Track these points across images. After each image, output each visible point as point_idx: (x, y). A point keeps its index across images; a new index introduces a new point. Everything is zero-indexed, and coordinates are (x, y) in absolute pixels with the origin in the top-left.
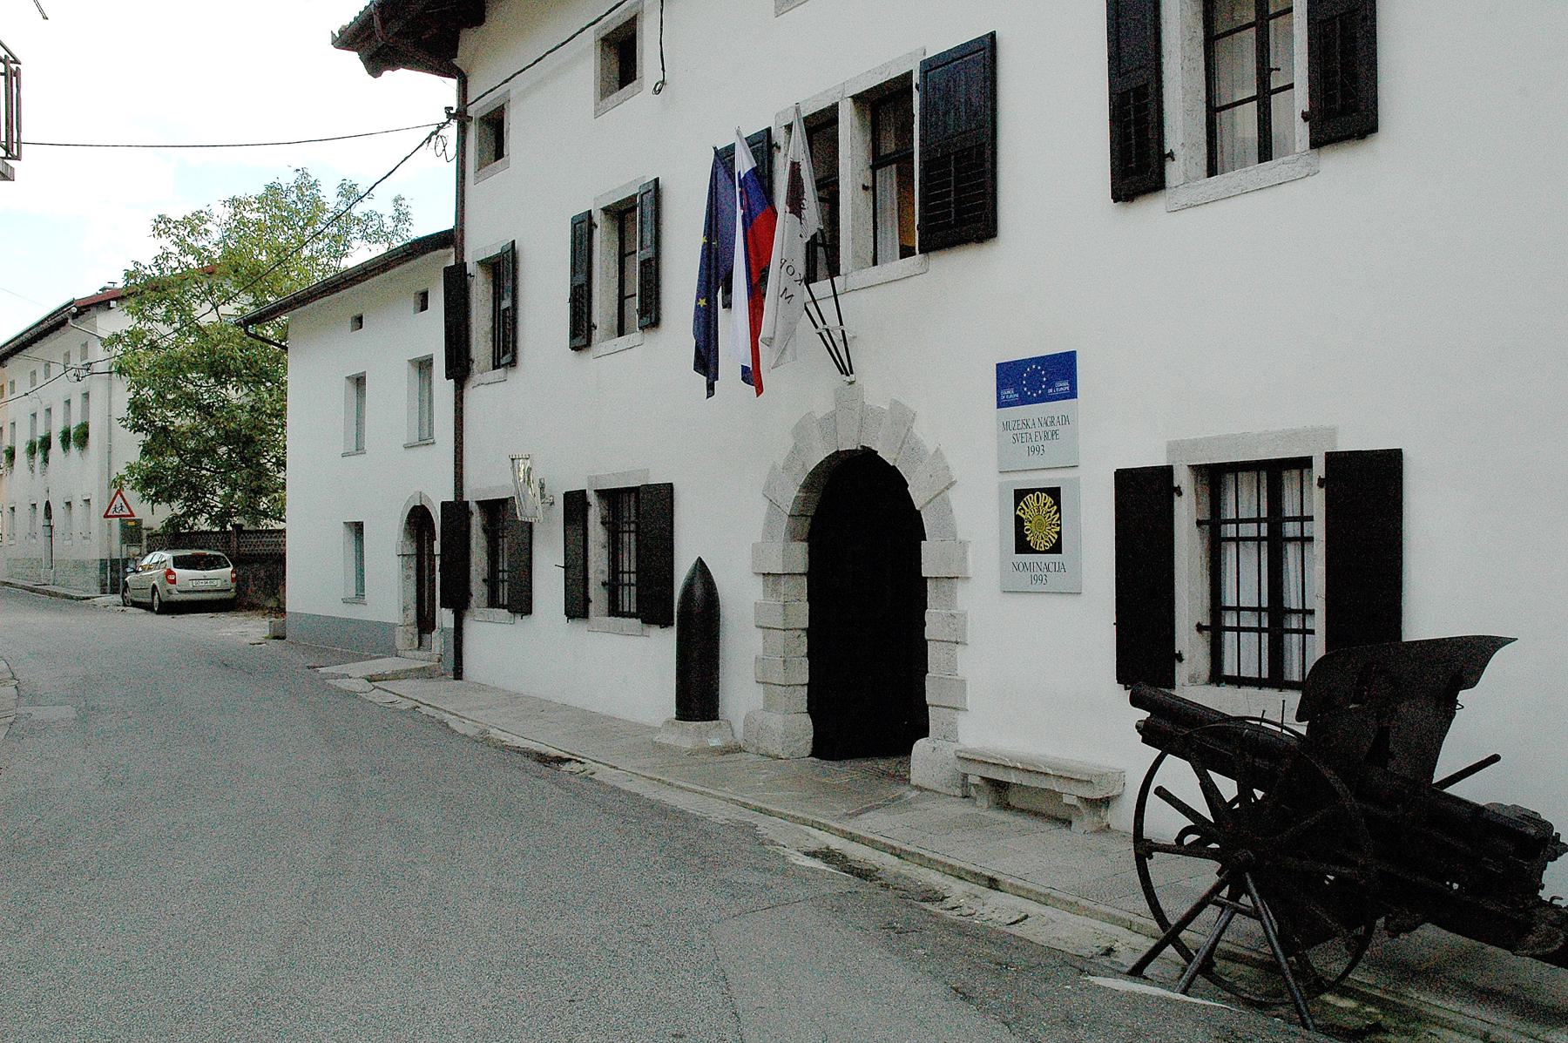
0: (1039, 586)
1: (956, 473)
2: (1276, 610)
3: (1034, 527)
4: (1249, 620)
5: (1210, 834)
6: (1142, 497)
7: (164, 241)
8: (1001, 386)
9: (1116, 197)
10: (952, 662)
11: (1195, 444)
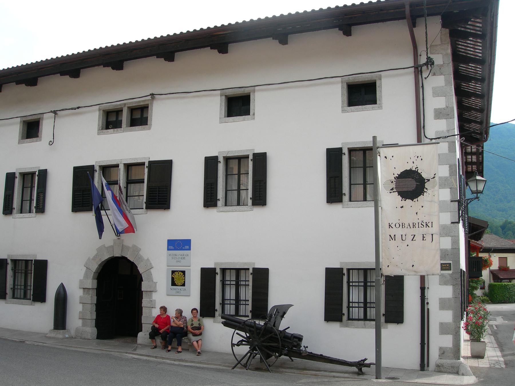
0: (178, 294)
1: (153, 265)
3: (178, 279)
4: (232, 302)
6: (207, 275)
9: (205, 206)
11: (222, 264)
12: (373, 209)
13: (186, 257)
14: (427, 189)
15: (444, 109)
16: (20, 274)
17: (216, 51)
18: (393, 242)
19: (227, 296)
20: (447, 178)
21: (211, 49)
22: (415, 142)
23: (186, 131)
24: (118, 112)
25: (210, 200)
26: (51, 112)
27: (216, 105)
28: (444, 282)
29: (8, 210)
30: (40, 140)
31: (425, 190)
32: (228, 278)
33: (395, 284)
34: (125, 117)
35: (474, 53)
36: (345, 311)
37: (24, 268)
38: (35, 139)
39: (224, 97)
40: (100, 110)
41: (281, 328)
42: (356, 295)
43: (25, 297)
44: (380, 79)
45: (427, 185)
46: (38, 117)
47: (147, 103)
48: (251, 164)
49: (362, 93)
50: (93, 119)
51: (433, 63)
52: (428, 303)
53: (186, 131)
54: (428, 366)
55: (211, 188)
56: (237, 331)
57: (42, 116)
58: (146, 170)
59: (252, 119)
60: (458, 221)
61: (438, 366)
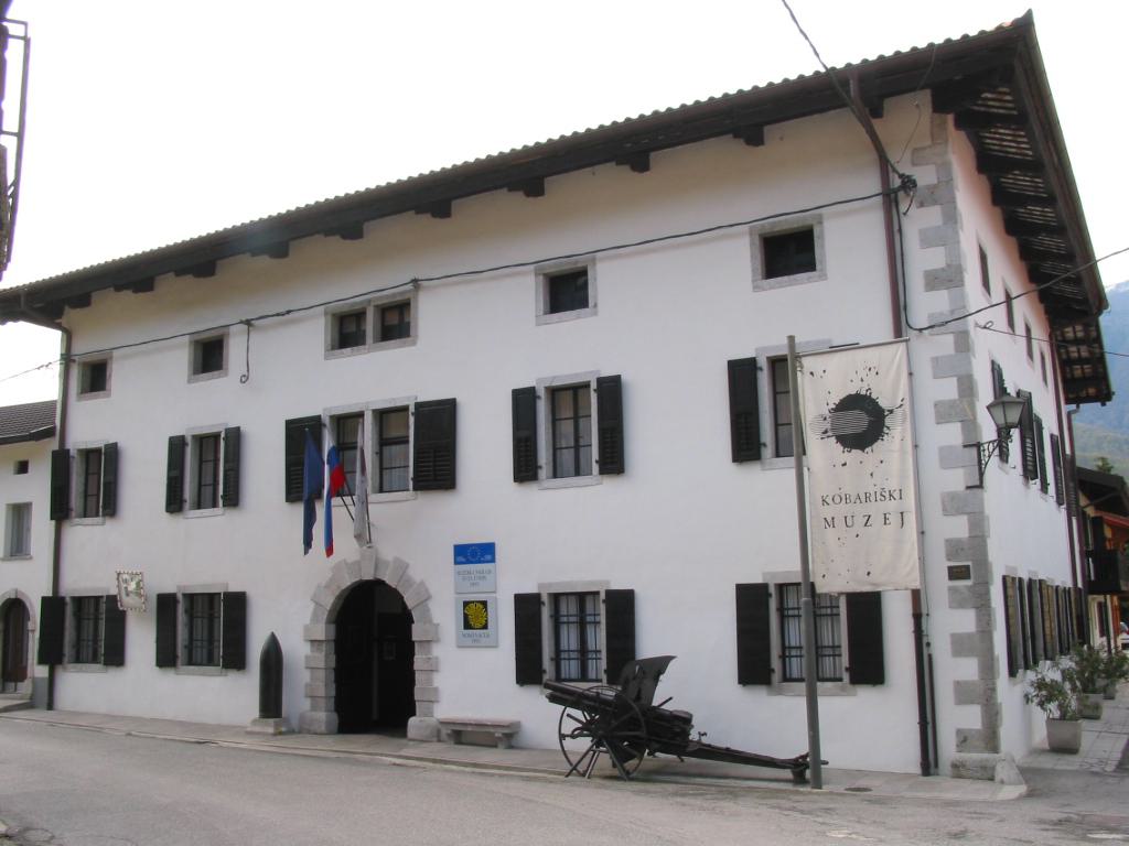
0: (476, 645)
2: (583, 651)
3: (474, 617)
4: (573, 655)
5: (586, 729)
6: (527, 606)
7: (1013, 394)
10: (430, 681)
11: (550, 585)
12: (793, 472)
13: (488, 576)
14: (888, 428)
15: (943, 269)
16: (199, 621)
17: (626, 168)
18: (830, 530)
19: (564, 645)
20: (955, 401)
22: (889, 335)
23: (478, 347)
24: (359, 316)
25: (525, 470)
26: (241, 322)
27: (528, 292)
28: (957, 602)
30: (226, 375)
31: (885, 430)
32: (563, 610)
33: (866, 609)
34: (370, 325)
35: (1019, 151)
36: (776, 663)
37: (92, 610)
38: (216, 373)
39: (541, 277)
40: (326, 313)
41: (655, 703)
42: (797, 633)
43: (210, 661)
44: (821, 223)
45: (887, 421)
46: (220, 332)
47: (406, 297)
48: (594, 398)
49: (788, 252)
50: (317, 331)
51: (914, 184)
52: (928, 644)
53: (478, 347)
54: (936, 765)
55: (527, 446)
56: (570, 710)
57: (225, 330)
59: (592, 315)
60: (978, 483)
61: (955, 766)
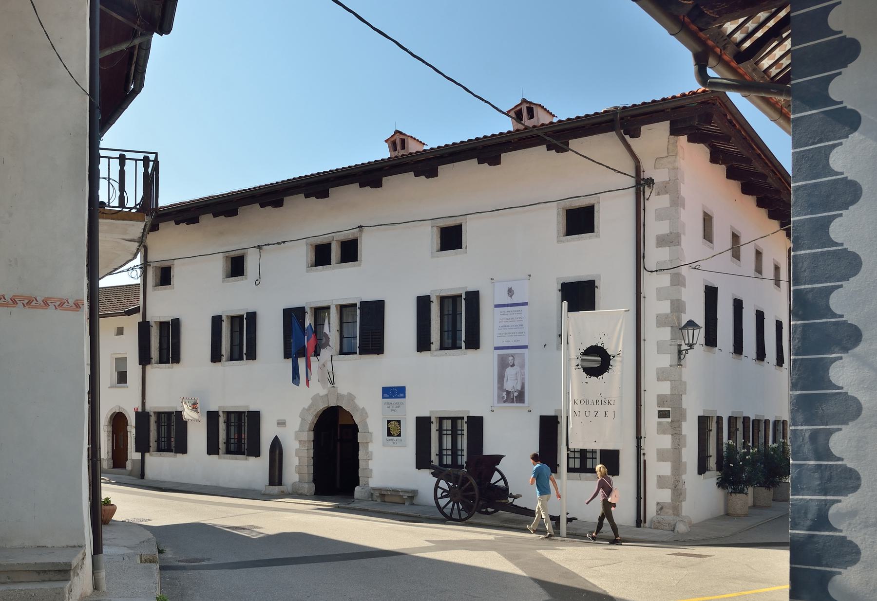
3: (393, 429)
8: (383, 393)
10: (367, 465)
11: (437, 412)
21: (689, 140)
29: (216, 357)
39: (435, 229)
49: (580, 221)
52: (644, 454)
54: (645, 522)
58: (358, 311)
